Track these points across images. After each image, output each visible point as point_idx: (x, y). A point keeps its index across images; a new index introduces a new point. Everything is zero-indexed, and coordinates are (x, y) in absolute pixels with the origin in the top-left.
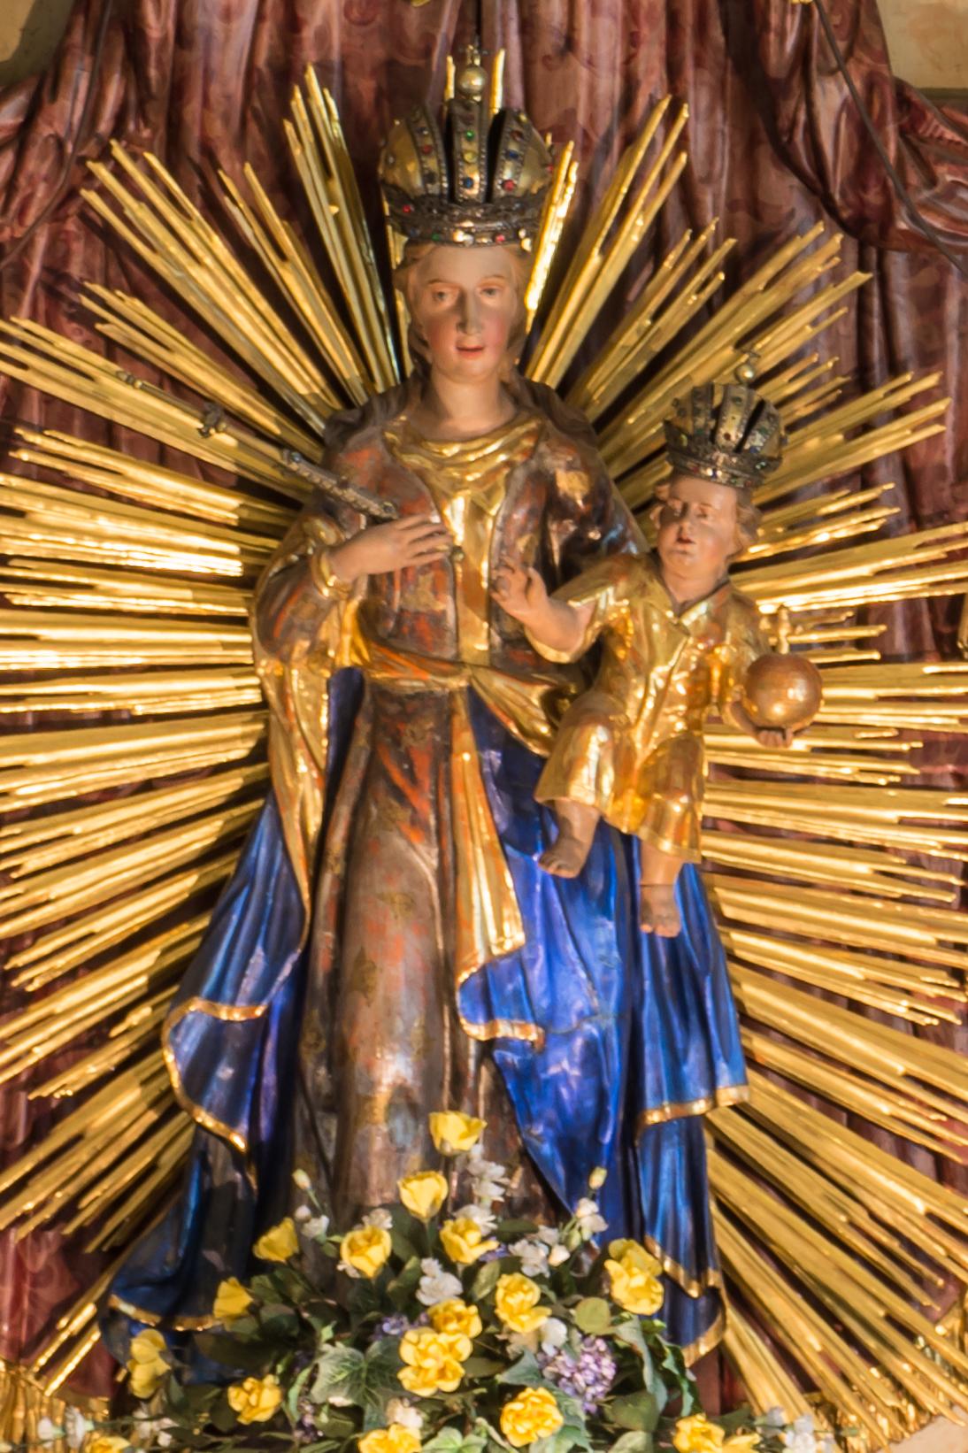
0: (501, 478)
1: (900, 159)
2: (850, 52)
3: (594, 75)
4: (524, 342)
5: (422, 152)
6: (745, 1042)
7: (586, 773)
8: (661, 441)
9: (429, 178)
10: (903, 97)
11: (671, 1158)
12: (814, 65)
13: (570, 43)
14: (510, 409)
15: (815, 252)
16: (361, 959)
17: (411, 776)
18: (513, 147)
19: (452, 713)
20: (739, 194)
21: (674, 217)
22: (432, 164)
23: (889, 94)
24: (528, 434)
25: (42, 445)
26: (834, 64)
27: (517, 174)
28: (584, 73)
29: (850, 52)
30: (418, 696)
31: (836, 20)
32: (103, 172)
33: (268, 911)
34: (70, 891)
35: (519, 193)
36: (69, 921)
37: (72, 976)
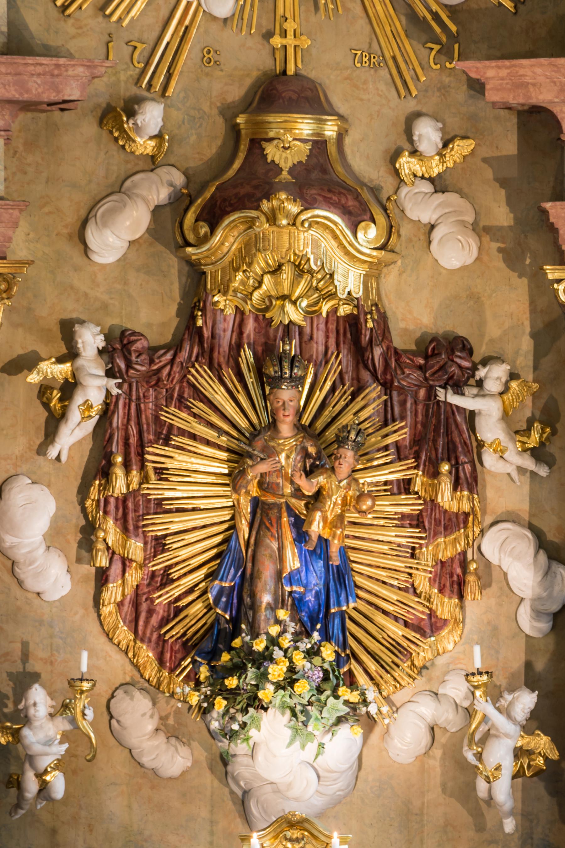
0: (294, 448)
1: (395, 367)
3: (317, 346)
4: (300, 414)
7: (315, 524)
8: (335, 439)
11: (337, 621)
13: (311, 338)
14: (296, 431)
16: (258, 570)
17: (271, 524)
18: (297, 364)
19: (281, 508)
20: (354, 376)
21: (338, 382)
22: (276, 368)
28: (315, 345)
29: (383, 340)
30: (273, 504)
31: (379, 332)
34: (184, 553)
36: (184, 561)
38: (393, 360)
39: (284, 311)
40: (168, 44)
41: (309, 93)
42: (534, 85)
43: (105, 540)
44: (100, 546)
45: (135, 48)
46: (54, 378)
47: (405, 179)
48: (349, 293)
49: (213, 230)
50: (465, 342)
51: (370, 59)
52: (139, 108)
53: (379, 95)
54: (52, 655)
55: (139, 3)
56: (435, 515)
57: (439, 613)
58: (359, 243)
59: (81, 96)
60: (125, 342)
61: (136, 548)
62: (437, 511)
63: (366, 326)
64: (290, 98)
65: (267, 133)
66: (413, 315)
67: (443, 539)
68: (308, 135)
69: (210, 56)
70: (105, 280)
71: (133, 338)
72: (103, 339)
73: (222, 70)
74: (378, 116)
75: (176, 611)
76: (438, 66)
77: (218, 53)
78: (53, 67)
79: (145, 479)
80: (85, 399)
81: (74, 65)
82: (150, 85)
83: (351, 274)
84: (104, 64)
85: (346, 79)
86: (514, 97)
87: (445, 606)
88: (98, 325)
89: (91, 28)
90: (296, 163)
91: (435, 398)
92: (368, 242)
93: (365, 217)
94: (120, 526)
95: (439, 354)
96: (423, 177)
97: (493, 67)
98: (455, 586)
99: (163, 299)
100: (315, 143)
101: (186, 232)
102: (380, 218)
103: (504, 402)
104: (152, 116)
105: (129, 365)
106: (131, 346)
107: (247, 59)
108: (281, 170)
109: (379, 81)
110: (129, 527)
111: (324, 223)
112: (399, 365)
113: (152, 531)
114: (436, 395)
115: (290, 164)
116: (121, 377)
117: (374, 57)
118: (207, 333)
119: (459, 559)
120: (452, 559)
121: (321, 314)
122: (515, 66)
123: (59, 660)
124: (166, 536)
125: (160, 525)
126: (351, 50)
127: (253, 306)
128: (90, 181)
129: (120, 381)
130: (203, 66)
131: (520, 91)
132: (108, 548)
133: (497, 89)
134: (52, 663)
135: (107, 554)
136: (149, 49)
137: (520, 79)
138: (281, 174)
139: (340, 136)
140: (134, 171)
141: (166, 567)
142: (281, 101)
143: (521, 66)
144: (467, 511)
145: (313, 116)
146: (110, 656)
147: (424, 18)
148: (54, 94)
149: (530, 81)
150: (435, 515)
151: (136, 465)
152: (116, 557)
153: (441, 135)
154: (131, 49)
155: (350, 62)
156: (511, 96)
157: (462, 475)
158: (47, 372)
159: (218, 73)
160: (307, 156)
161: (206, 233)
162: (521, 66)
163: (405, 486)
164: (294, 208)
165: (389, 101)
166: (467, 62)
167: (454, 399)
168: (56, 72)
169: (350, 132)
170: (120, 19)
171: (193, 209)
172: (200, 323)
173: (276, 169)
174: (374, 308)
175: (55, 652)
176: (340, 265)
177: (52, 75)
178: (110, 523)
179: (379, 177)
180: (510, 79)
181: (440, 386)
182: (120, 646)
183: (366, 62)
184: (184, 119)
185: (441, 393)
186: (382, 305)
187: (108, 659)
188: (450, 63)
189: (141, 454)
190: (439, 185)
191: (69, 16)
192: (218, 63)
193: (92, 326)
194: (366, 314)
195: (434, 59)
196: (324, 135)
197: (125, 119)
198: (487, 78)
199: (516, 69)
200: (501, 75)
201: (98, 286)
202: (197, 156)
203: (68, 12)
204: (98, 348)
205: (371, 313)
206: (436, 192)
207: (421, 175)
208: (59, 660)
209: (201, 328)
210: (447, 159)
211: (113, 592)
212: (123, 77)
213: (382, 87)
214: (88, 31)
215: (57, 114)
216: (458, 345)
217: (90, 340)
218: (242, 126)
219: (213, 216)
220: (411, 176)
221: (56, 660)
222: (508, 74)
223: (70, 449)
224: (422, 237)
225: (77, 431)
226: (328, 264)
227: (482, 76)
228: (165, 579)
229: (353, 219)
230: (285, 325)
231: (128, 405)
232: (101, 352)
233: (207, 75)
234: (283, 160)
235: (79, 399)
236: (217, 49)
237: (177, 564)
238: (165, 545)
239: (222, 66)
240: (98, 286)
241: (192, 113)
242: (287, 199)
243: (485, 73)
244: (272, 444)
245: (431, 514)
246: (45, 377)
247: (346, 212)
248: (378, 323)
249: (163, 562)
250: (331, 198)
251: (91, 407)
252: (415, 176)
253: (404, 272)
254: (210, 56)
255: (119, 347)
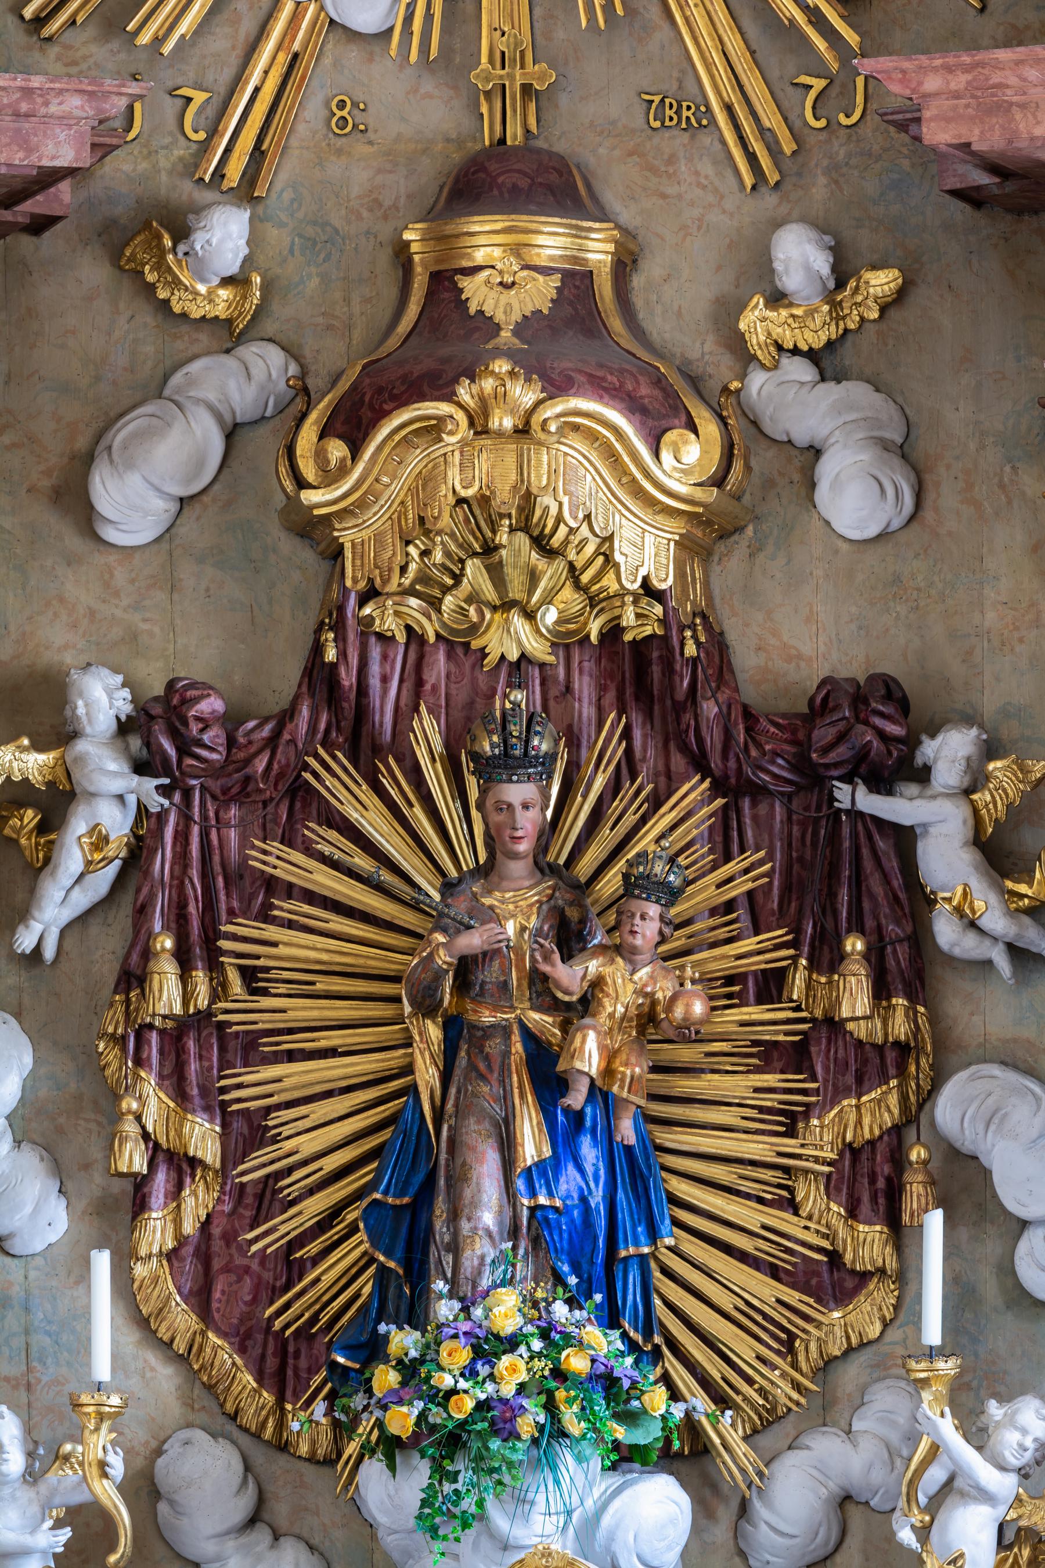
0: (535, 909)
1: (746, 744)
2: (718, 688)
3: (581, 706)
4: (542, 846)
5: (490, 733)
6: (660, 1160)
8: (621, 891)
9: (493, 746)
10: (748, 714)
11: (634, 1276)
12: (699, 694)
13: (568, 689)
14: (539, 875)
15: (693, 790)
16: (464, 1164)
17: (490, 1067)
18: (538, 729)
19: (511, 1032)
20: (661, 767)
21: (624, 771)
22: (495, 739)
23: (740, 709)
24: (549, 887)
25: (284, 907)
26: (710, 694)
27: (541, 742)
28: (577, 705)
31: (710, 672)
32: (311, 761)
33: (583, 234)
34: (308, 1144)
35: (541, 754)
36: (305, 1163)
37: (311, 1191)
38: (741, 726)
39: (509, 631)
40: (257, 90)
41: (554, 177)
42: (1023, 106)
43: (138, 1118)
44: (130, 1127)
45: (189, 100)
46: (26, 781)
47: (759, 353)
48: (646, 580)
49: (355, 452)
50: (891, 684)
51: (678, 112)
52: (199, 221)
53: (699, 185)
54: (29, 1369)
55: (195, 8)
56: (836, 1052)
57: (848, 1257)
58: (664, 471)
59: (76, 160)
60: (175, 701)
61: (203, 1138)
62: (840, 1043)
63: (682, 654)
64: (515, 186)
65: (469, 257)
66: (793, 636)
67: (854, 1102)
68: (552, 258)
69: (344, 113)
70: (132, 581)
71: (190, 693)
72: (130, 698)
73: (371, 143)
74: (699, 228)
75: (291, 1264)
76: (822, 123)
77: (362, 106)
78: (18, 95)
79: (219, 990)
80: (92, 824)
81: (61, 92)
82: (219, 174)
83: (649, 539)
84: (124, 90)
85: (631, 154)
86: (982, 132)
87: (868, 1244)
88: (116, 671)
89: (95, 63)
90: (528, 314)
91: (830, 805)
92: (682, 471)
93: (677, 422)
94: (170, 1089)
95: (837, 707)
96: (795, 351)
97: (935, 69)
98: (881, 1201)
99: (253, 618)
100: (568, 276)
101: (301, 463)
102: (709, 428)
103: (976, 812)
104: (225, 236)
105: (184, 749)
106: (189, 709)
107: (422, 116)
108: (498, 328)
109: (701, 159)
110: (188, 1089)
111: (589, 428)
112: (750, 736)
113: (239, 1100)
114: (832, 799)
115: (516, 316)
116: (167, 772)
117: (689, 108)
118: (348, 678)
119: (889, 1144)
120: (872, 1143)
121: (588, 636)
122: (982, 64)
123: (45, 1379)
124: (268, 1110)
125: (256, 1083)
126: (639, 95)
127: (444, 625)
128: (98, 379)
129: (166, 781)
130: (331, 135)
131: (994, 120)
132: (146, 1136)
133: (946, 119)
134: (29, 1387)
135: (143, 1147)
136: (217, 101)
137: (993, 95)
138: (498, 335)
139: (624, 265)
140: (190, 353)
141: (268, 1176)
142: (495, 192)
143: (998, 66)
144: (903, 1038)
145: (564, 221)
146: (153, 1369)
147: (792, 21)
148: (21, 154)
149: (1015, 99)
150: (836, 1052)
151: (202, 960)
152: (161, 1157)
153: (831, 260)
154: (179, 102)
155: (640, 121)
156: (977, 132)
157: (891, 963)
158: (11, 766)
159: (362, 149)
160: (552, 300)
161: (343, 460)
162: (998, 66)
163: (770, 986)
164: (524, 394)
165: (722, 197)
166: (881, 59)
167: (869, 802)
168: (24, 107)
169: (643, 264)
170: (158, 41)
171: (313, 416)
172: (331, 654)
173: (487, 326)
174: (698, 621)
175: (35, 1364)
176: (624, 521)
177: (17, 114)
178: (149, 1084)
179: (703, 354)
180: (973, 97)
181: (840, 779)
182: (175, 1346)
183: (671, 119)
184: (293, 243)
185: (843, 793)
186: (716, 618)
187: (148, 1375)
188: (848, 116)
189: (211, 935)
190: (826, 361)
191: (49, 39)
192: (362, 127)
193: (105, 672)
194: (682, 628)
195: (814, 108)
196: (586, 260)
197: (168, 243)
198: (925, 96)
199: (986, 72)
200: (953, 86)
201: (117, 594)
202: (320, 320)
203: (46, 32)
204: (118, 718)
205: (693, 627)
206: (823, 379)
207: (791, 347)
208: (45, 1379)
209: (334, 666)
210: (846, 311)
211: (156, 1232)
212: (164, 163)
213: (706, 168)
214: (89, 68)
215: (26, 242)
216: (890, 691)
217: (101, 700)
218: (415, 248)
219: (353, 424)
220: (772, 349)
221: (39, 1381)
222: (968, 83)
223: (63, 932)
224: (796, 477)
225: (76, 893)
226: (600, 519)
227: (914, 91)
228: (265, 1199)
229: (650, 423)
230: (510, 663)
231: (182, 837)
232: (124, 728)
233: (339, 152)
234: (502, 310)
235: (78, 826)
236: (361, 98)
237: (290, 1170)
238: (268, 1129)
239: (370, 134)
240: (117, 594)
241: (310, 231)
242: (512, 374)
243: (920, 83)
244: (487, 901)
245: (829, 1051)
246: (8, 778)
247: (634, 407)
248: (707, 654)
249: (264, 1165)
250: (603, 379)
251: (106, 840)
252: (780, 348)
253: (760, 550)
254: (344, 113)
255: (156, 730)
